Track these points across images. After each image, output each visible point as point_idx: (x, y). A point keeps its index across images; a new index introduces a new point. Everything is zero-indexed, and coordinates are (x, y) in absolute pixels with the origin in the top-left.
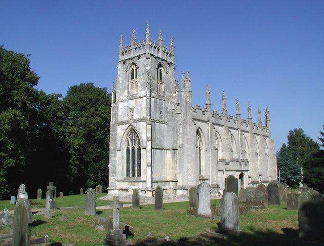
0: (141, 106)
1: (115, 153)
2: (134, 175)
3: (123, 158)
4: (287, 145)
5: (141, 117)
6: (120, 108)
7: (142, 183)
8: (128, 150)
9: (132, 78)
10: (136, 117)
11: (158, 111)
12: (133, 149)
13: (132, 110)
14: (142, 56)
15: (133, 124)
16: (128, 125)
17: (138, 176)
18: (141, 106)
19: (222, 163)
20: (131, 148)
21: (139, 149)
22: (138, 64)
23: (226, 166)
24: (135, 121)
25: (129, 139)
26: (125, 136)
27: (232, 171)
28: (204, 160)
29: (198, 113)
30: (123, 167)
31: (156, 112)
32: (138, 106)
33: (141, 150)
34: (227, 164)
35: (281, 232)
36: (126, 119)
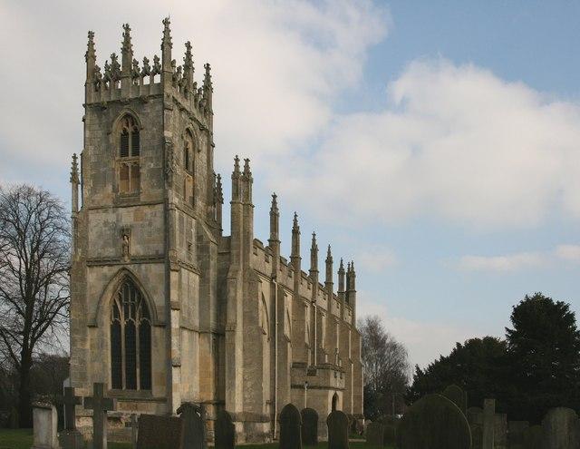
0: (150, 224)
1: (85, 332)
2: (132, 385)
3: (101, 345)
4: (512, 327)
5: (152, 253)
6: (92, 225)
7: (154, 405)
8: (115, 327)
9: (124, 153)
10: (136, 249)
11: (185, 243)
12: (130, 326)
13: (125, 232)
14: (152, 101)
15: (131, 267)
16: (115, 269)
17: (142, 387)
18: (150, 224)
19: (298, 371)
20: (123, 323)
21: (146, 329)
22: (142, 121)
23: (308, 379)
24: (135, 260)
25: (118, 303)
26: (109, 295)
27: (320, 388)
28: (289, 365)
29: (259, 257)
30: (105, 366)
31: (181, 244)
32: (142, 226)
33: (152, 327)
34: (312, 373)
35: (556, 304)
36: (110, 252)
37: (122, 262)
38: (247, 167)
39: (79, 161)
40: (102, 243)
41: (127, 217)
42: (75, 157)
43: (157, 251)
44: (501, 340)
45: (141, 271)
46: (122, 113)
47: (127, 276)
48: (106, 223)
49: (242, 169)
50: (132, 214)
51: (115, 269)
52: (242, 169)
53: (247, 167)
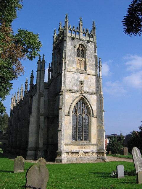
5: (91, 91)
7: (92, 146)
13: (82, 83)
35: (11, 82)
36: (75, 88)
37: (81, 92)
38: (43, 58)
39: (51, 65)
40: (72, 84)
41: (82, 77)
42: (50, 64)
43: (93, 91)
44: (62, 155)
45: (88, 97)
46: (80, 43)
47: (82, 98)
48: (73, 78)
49: (42, 59)
50: (84, 77)
51: (78, 95)
52: (42, 59)
53: (43, 58)
